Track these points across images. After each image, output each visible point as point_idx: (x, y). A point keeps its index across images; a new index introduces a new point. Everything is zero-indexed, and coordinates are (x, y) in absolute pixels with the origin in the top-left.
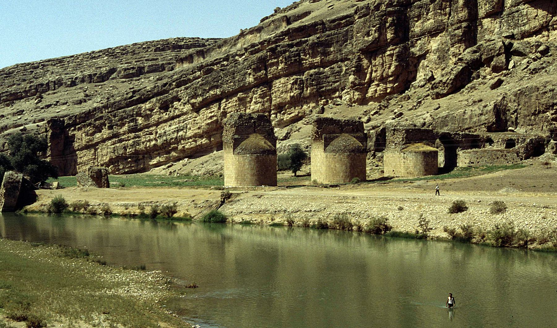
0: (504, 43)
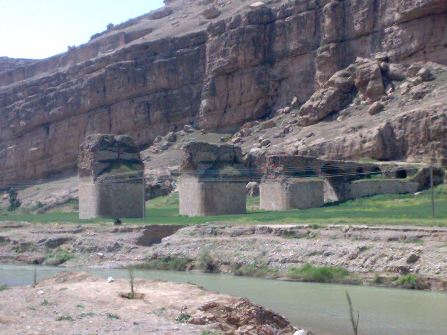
0: (379, 66)
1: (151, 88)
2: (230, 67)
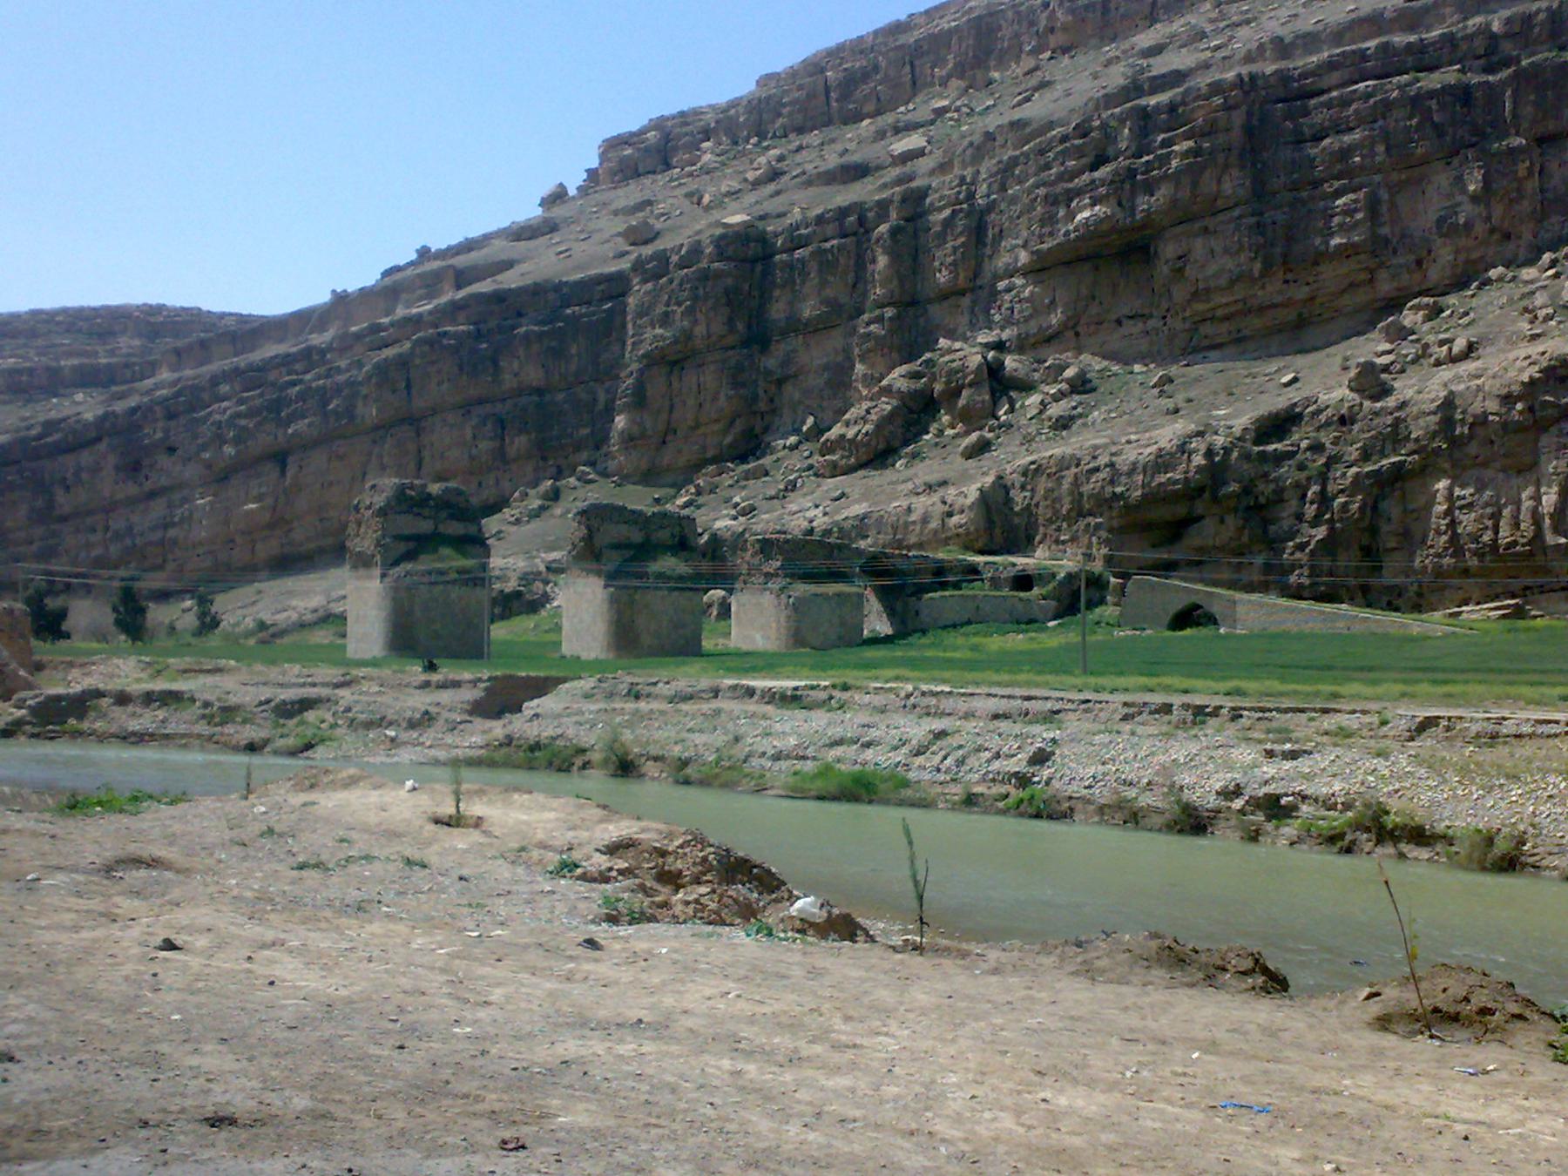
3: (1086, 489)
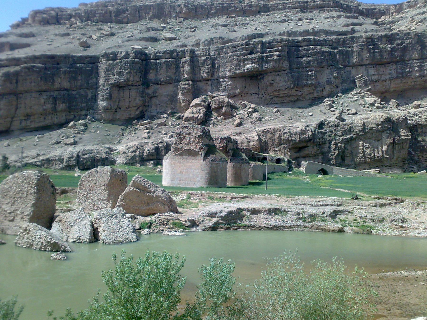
1: (57, 87)
2: (125, 83)
3: (283, 137)
